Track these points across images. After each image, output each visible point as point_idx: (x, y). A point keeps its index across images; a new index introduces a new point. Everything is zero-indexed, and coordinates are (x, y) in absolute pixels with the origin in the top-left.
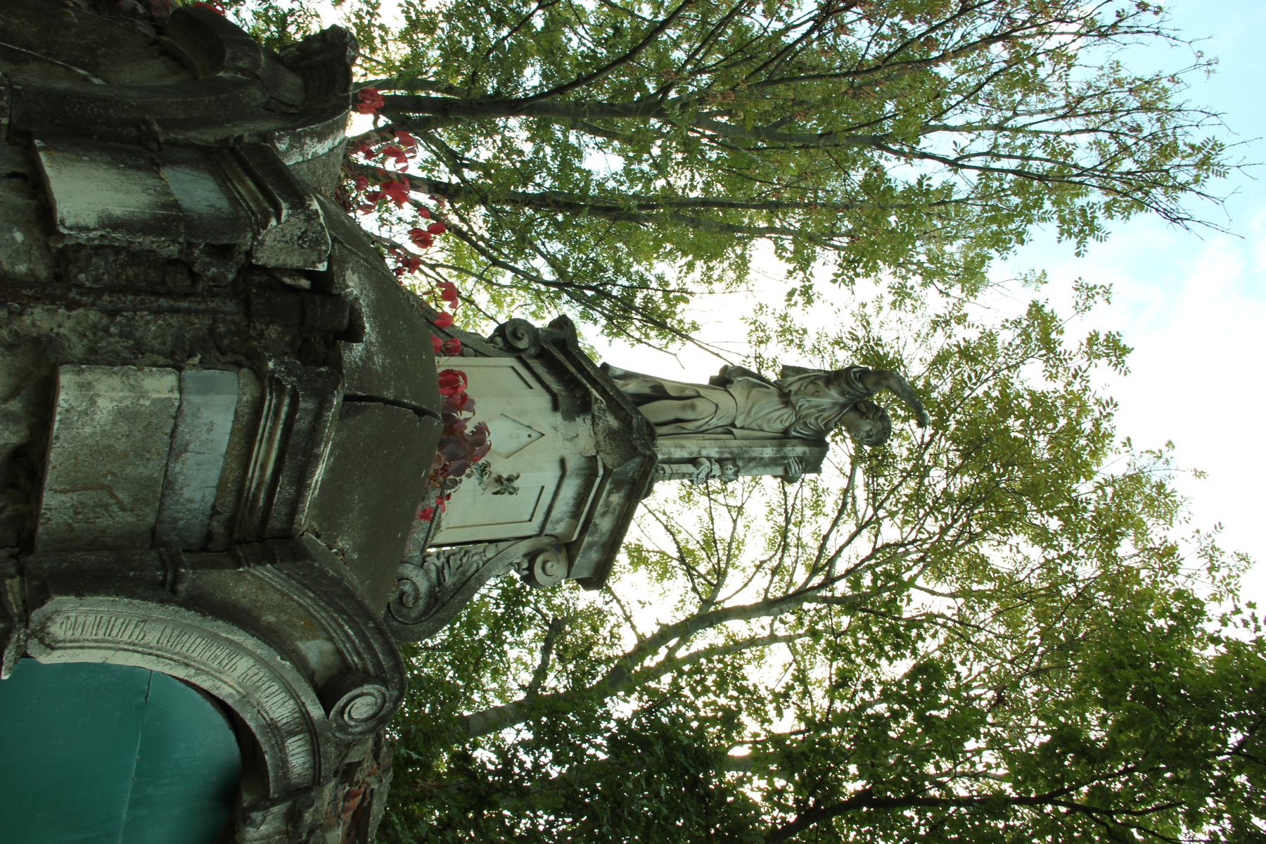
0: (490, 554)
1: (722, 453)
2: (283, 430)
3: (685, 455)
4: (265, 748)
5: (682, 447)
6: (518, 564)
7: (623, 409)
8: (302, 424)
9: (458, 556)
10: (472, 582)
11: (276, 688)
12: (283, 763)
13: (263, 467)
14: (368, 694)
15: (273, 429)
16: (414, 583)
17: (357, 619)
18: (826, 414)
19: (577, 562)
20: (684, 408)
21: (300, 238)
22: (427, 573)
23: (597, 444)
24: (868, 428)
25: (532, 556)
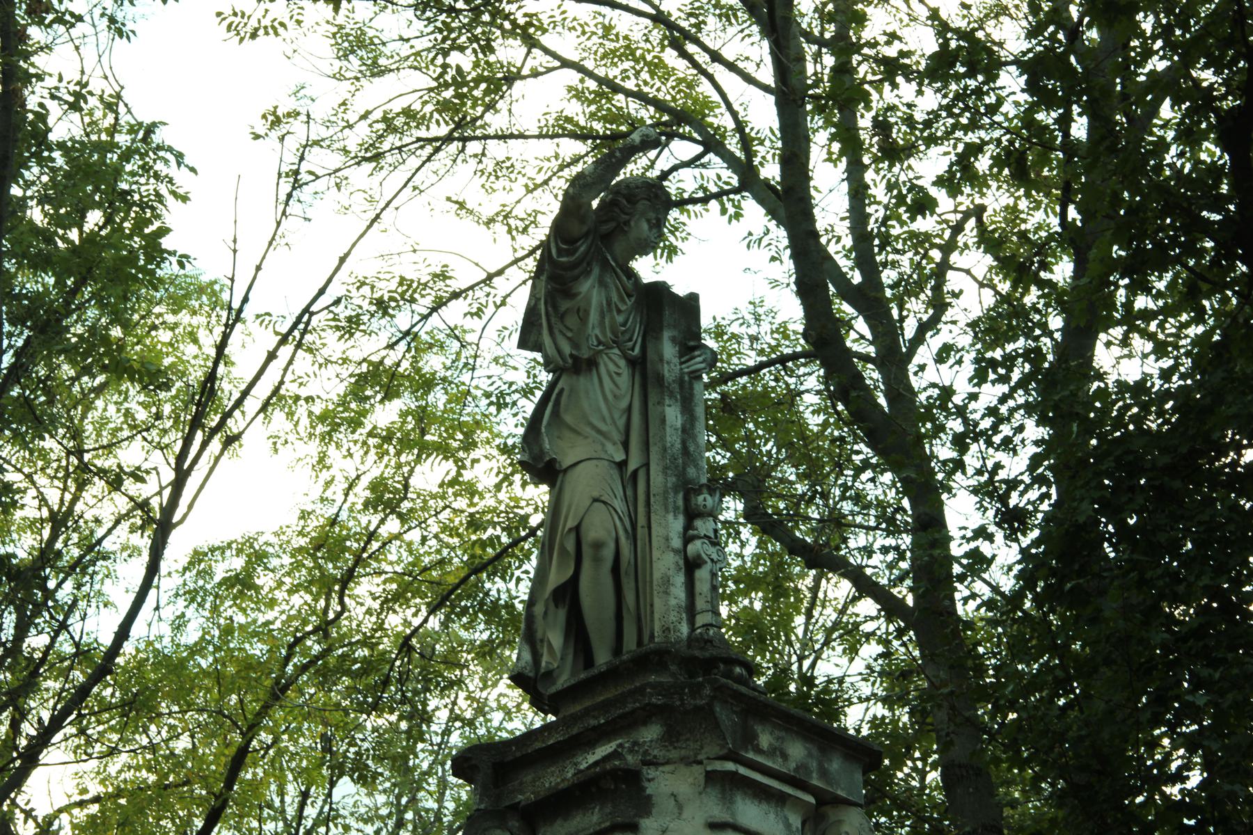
1: (676, 509)
3: (680, 579)
5: (667, 582)
7: (633, 712)
18: (615, 298)
20: (597, 560)
24: (645, 226)
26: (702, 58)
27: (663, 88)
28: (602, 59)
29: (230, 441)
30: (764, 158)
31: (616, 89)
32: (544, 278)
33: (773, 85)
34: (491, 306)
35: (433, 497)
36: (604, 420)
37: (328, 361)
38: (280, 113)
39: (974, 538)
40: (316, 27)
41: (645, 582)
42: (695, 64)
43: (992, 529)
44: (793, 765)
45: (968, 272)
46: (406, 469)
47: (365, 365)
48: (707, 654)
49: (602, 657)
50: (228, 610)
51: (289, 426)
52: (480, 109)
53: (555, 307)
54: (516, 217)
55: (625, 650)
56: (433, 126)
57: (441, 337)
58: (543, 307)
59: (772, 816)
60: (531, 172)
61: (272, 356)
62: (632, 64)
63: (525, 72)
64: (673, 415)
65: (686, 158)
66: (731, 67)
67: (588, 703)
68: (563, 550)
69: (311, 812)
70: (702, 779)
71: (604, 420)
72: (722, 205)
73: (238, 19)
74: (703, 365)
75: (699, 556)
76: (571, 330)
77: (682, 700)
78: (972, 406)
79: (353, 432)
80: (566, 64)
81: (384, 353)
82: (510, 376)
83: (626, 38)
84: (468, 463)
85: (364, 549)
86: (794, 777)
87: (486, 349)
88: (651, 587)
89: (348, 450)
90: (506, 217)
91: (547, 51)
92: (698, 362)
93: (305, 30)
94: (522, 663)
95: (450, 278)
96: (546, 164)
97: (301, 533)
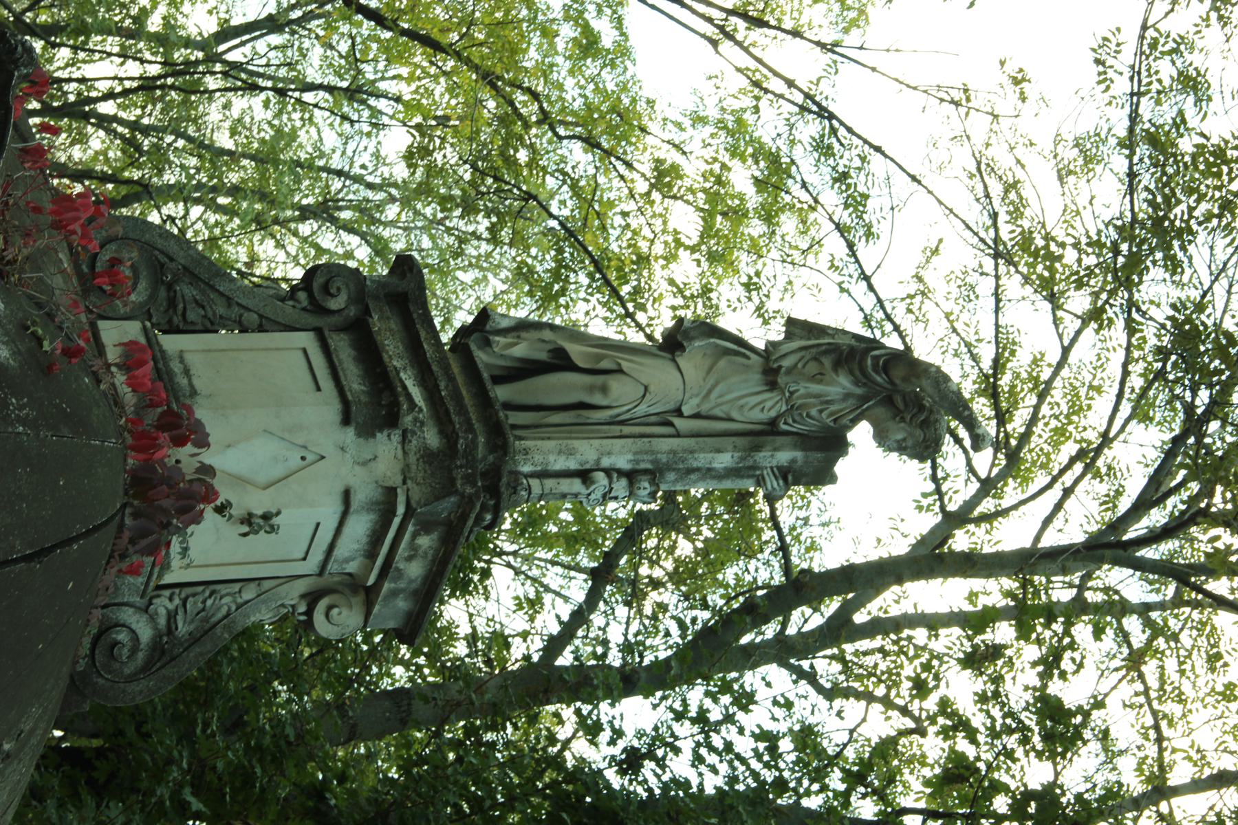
0: (247, 595)
1: (637, 462)
3: (573, 465)
5: (570, 453)
7: (451, 422)
9: (201, 598)
16: (133, 632)
18: (833, 408)
19: (376, 609)
20: (591, 389)
22: (153, 618)
24: (900, 436)
26: (1068, 479)
27: (1042, 440)
28: (1071, 384)
29: (714, 43)
30: (973, 534)
31: (1042, 397)
32: (853, 342)
33: (1040, 546)
34: (841, 279)
35: (665, 223)
36: (720, 396)
37: (791, 127)
38: (1024, 85)
39: (614, 730)
40: (1105, 119)
41: (571, 432)
42: (1062, 472)
43: (621, 744)
44: (401, 566)
45: (864, 720)
46: (690, 198)
47: (788, 160)
48: (503, 489)
49: (502, 393)
50: (567, 32)
51: (734, 91)
52: (1024, 270)
53: (825, 353)
54: (922, 302)
55: (509, 413)
56: (1010, 227)
57: (812, 232)
58: (826, 341)
59: (356, 546)
60: (965, 317)
61: (791, 84)
62: (1065, 412)
63: (1060, 313)
64: (724, 460)
65: (975, 463)
66: (1058, 507)
67: (460, 379)
68: (600, 358)
69: (382, 104)
70: (390, 484)
71: (720, 396)
72: (931, 494)
73: (1114, 48)
74: (769, 487)
75: (593, 483)
76: (804, 367)
77: (461, 467)
78: (734, 729)
79: (726, 149)
80: (1066, 351)
81: (798, 178)
82: (776, 295)
83: (1089, 407)
84: (697, 256)
85: (618, 158)
86: (390, 566)
87: (799, 274)
88: (567, 438)
89: (709, 144)
90: (923, 293)
91: (1078, 333)
92: (772, 482)
93: (1103, 108)
94: (498, 319)
95: (867, 241)
96: (972, 331)
97: (634, 101)
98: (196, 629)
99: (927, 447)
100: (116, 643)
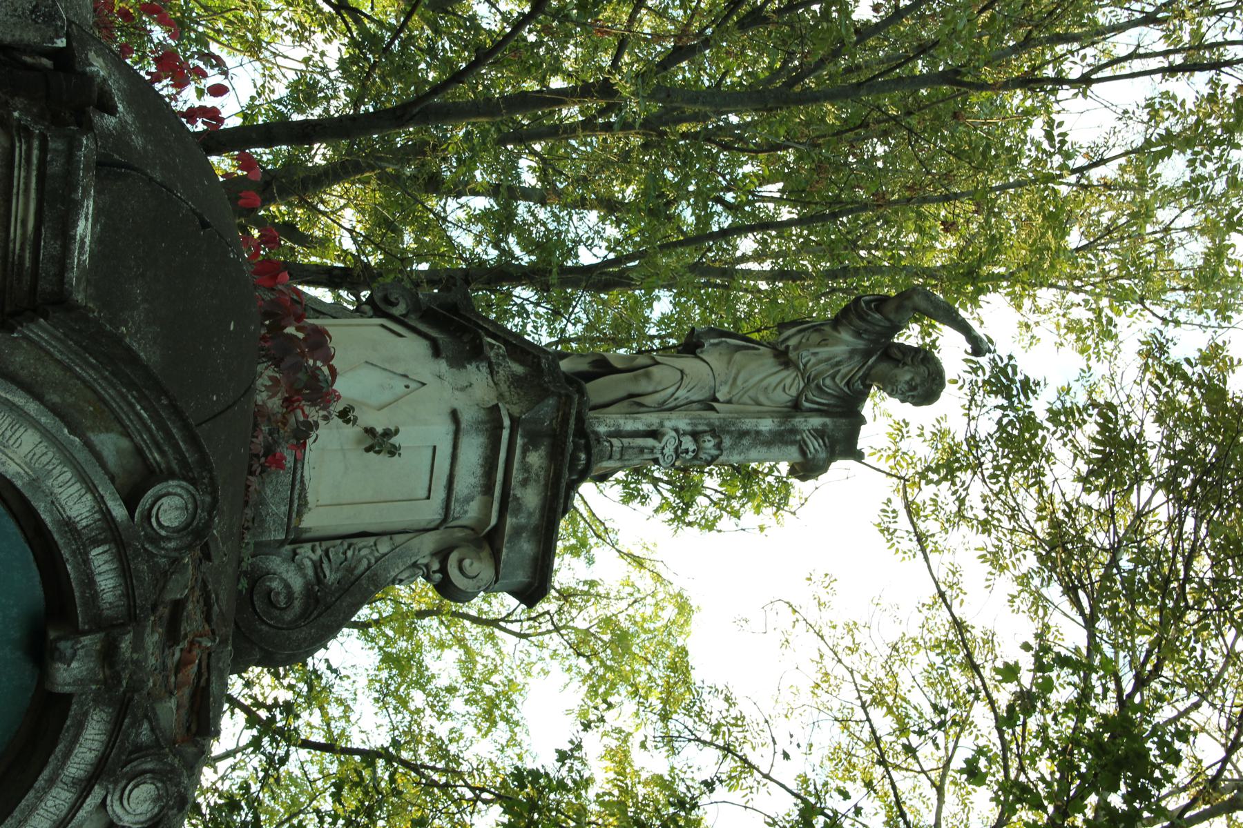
2: (37, 183)
3: (640, 426)
4: (66, 554)
6: (427, 566)
8: (55, 168)
10: (364, 581)
11: (69, 475)
12: (89, 581)
13: (24, 223)
14: (175, 494)
15: (28, 178)
17: (147, 392)
20: (636, 378)
21: (32, 12)
22: (300, 568)
23: (501, 396)
24: (908, 377)
25: (442, 555)
36: (745, 381)
59: (472, 480)
71: (745, 381)
98: (343, 577)
99: (934, 379)
100: (270, 591)
